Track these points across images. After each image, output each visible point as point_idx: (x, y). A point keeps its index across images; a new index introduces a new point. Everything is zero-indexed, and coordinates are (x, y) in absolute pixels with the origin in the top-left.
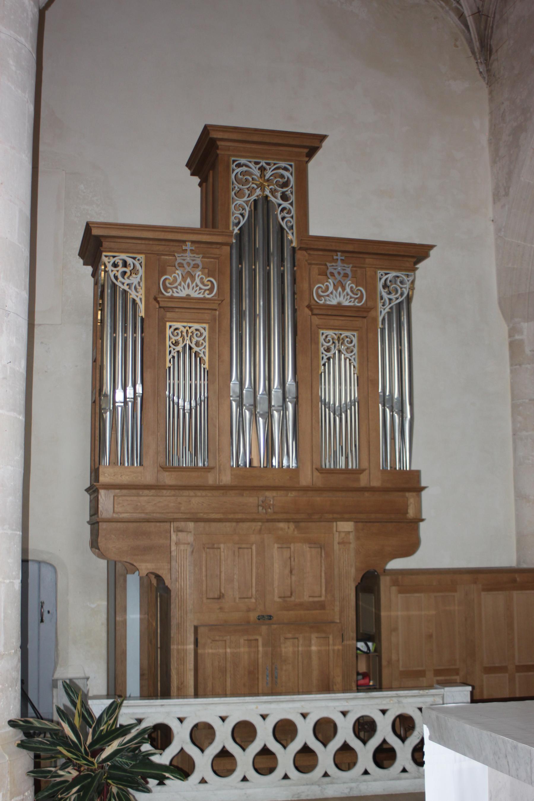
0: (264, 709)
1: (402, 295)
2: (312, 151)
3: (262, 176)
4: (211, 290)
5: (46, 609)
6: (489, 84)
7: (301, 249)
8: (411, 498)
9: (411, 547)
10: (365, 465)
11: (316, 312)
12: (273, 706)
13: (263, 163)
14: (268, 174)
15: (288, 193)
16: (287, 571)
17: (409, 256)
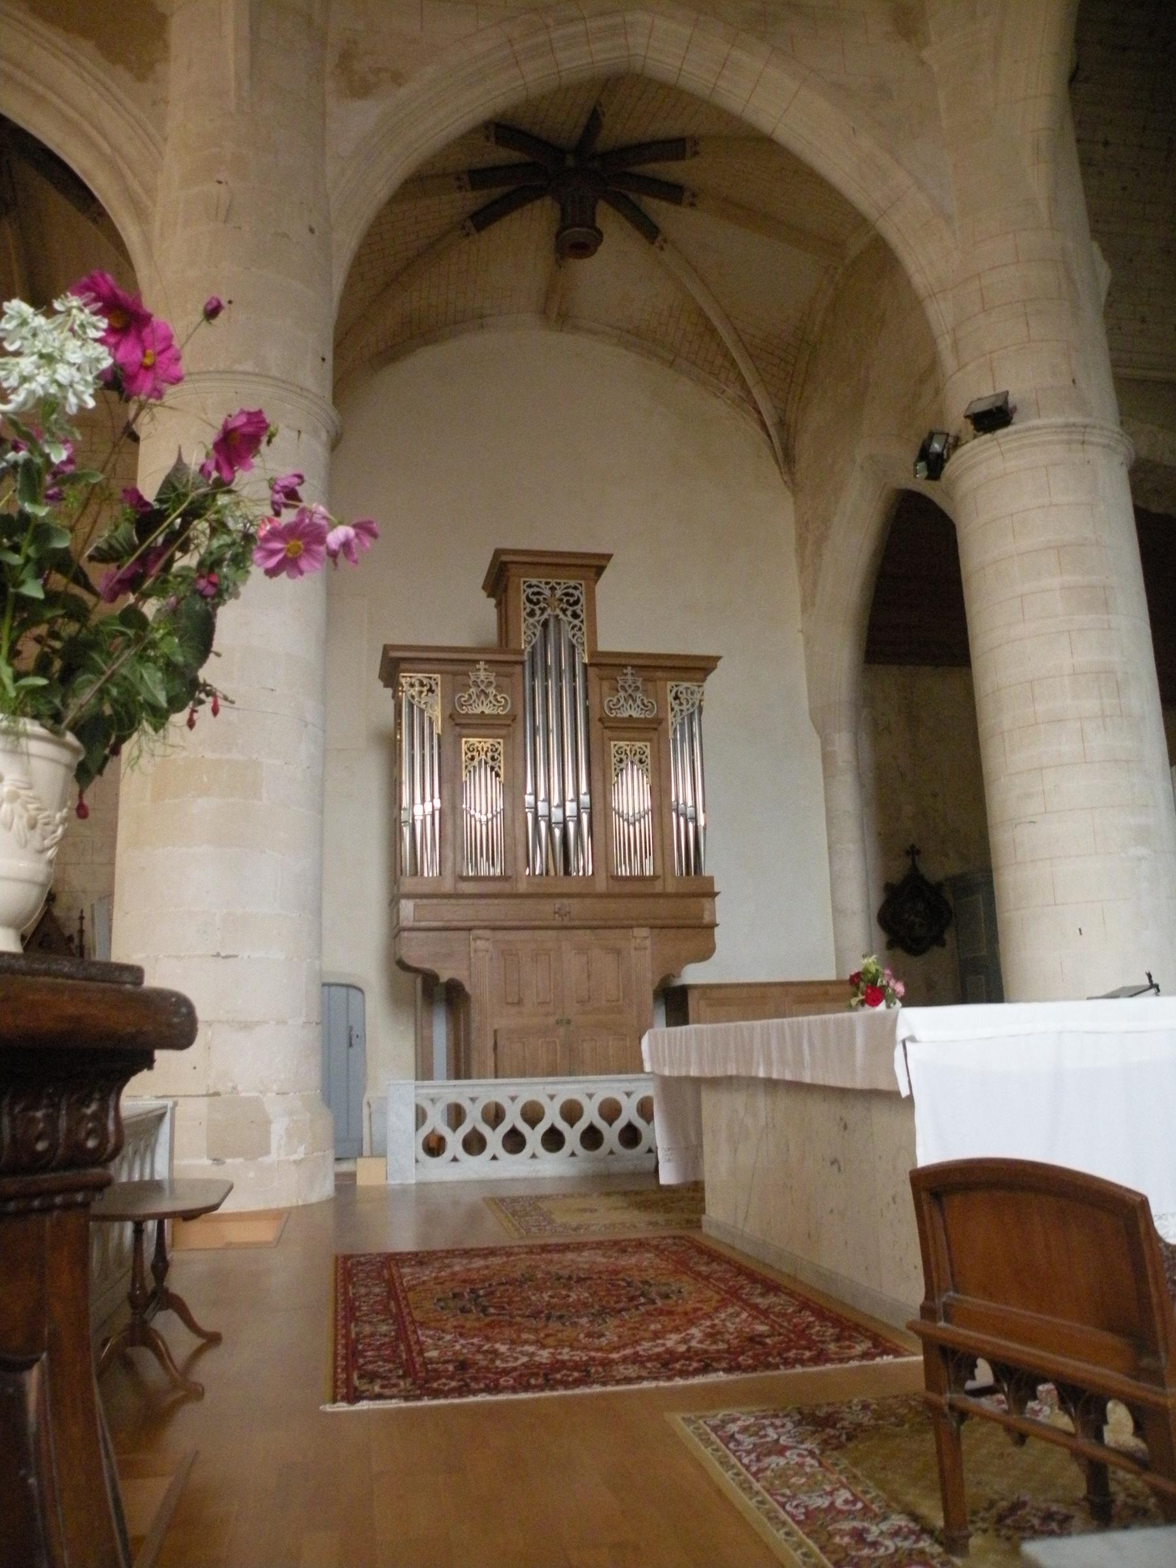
0: (551, 1089)
1: (693, 705)
2: (600, 570)
3: (553, 595)
4: (504, 707)
5: (354, 1033)
6: (794, 493)
7: (591, 665)
8: (706, 902)
9: (705, 952)
10: (660, 872)
11: (607, 724)
12: (560, 1087)
13: (553, 582)
14: (559, 593)
15: (579, 612)
16: (585, 976)
17: (698, 668)
